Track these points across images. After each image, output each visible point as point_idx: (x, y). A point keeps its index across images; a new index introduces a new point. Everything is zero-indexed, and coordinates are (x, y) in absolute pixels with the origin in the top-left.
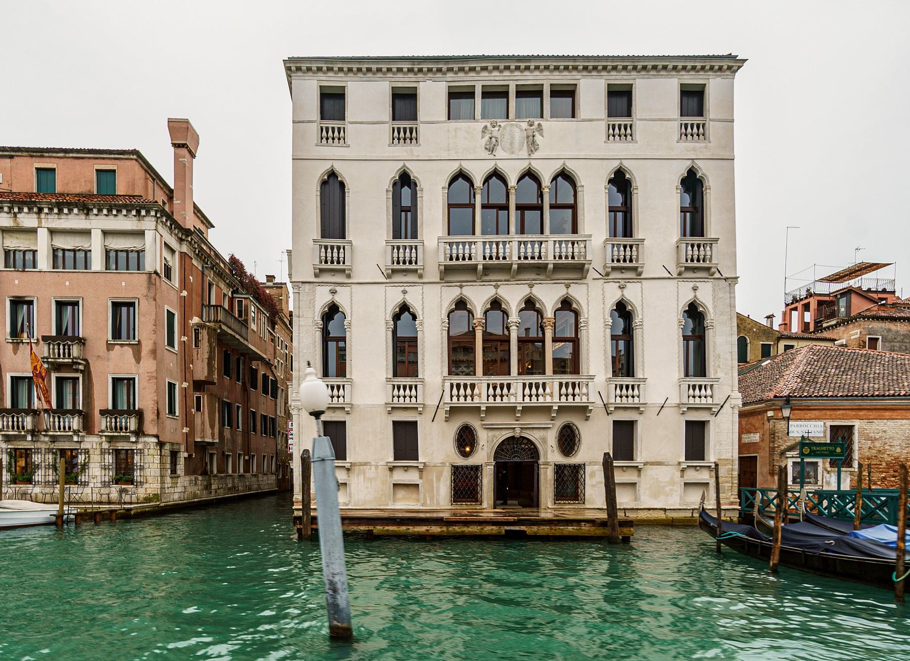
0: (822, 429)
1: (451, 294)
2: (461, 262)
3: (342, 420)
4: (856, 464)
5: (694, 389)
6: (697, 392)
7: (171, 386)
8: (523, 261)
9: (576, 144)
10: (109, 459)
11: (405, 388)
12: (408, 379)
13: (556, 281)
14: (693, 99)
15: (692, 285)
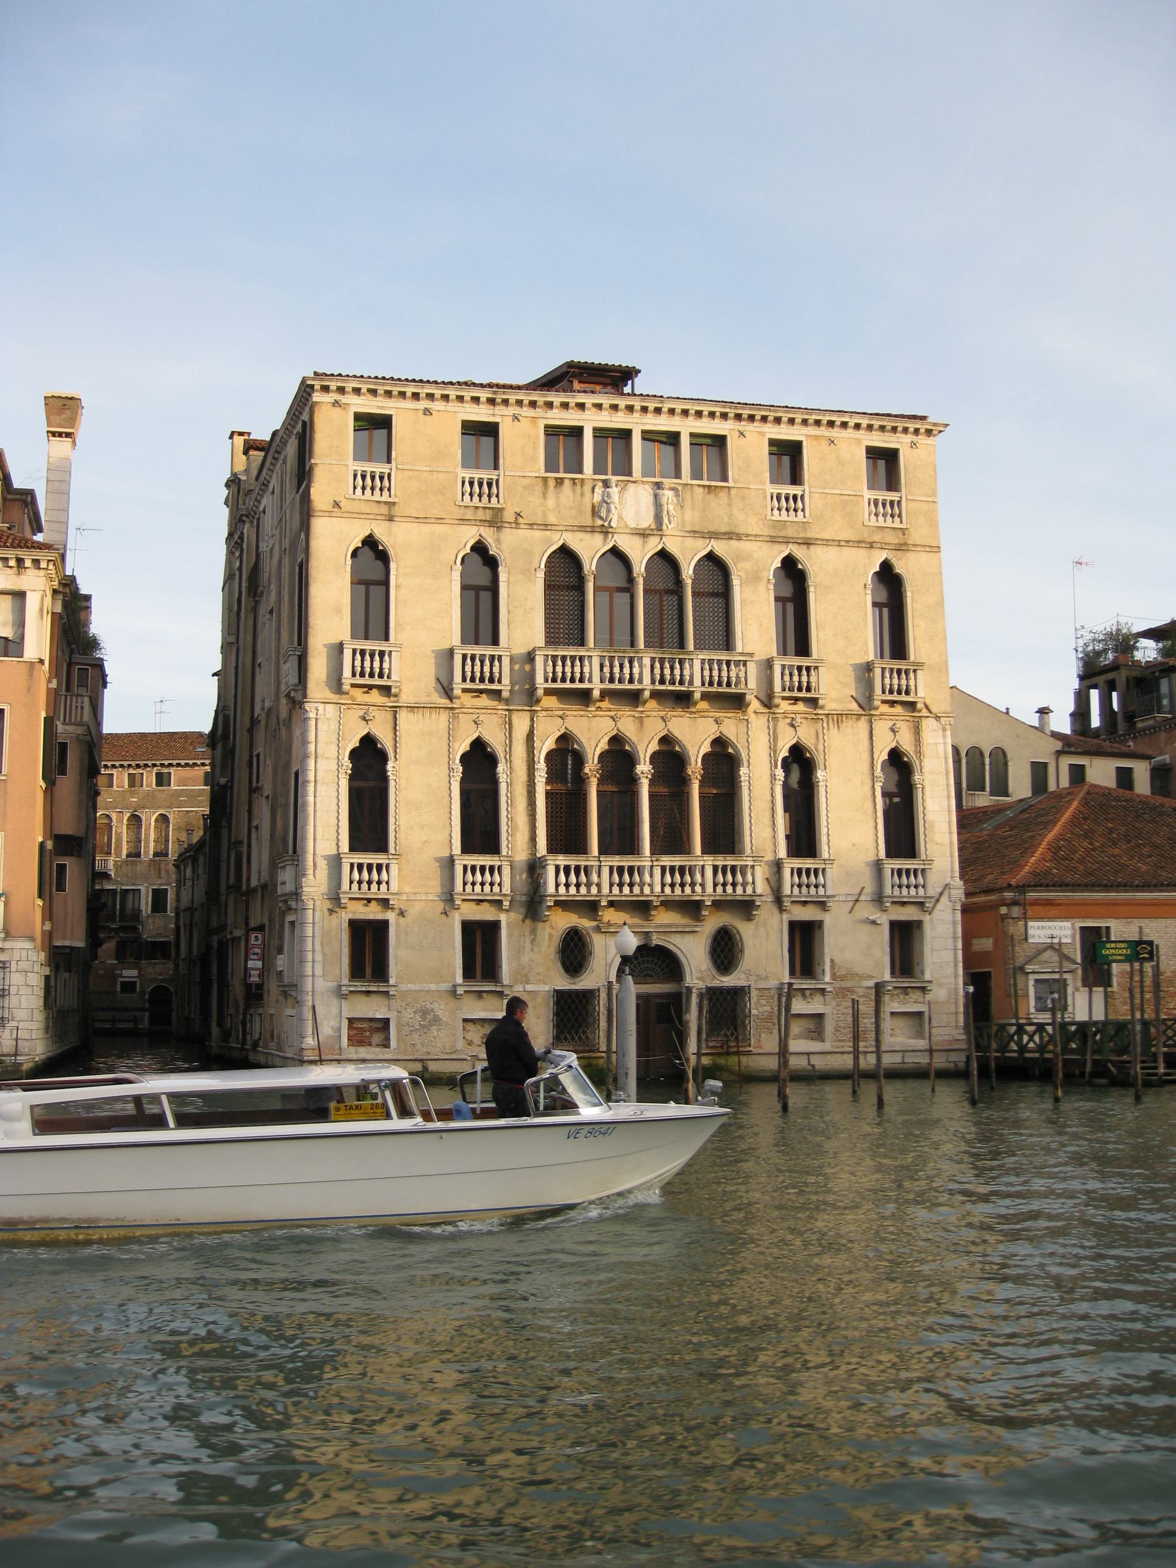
0: (1069, 932)
2: (568, 685)
5: (900, 875)
6: (904, 880)
9: (742, 522)
12: (481, 857)
14: (885, 463)
15: (890, 723)
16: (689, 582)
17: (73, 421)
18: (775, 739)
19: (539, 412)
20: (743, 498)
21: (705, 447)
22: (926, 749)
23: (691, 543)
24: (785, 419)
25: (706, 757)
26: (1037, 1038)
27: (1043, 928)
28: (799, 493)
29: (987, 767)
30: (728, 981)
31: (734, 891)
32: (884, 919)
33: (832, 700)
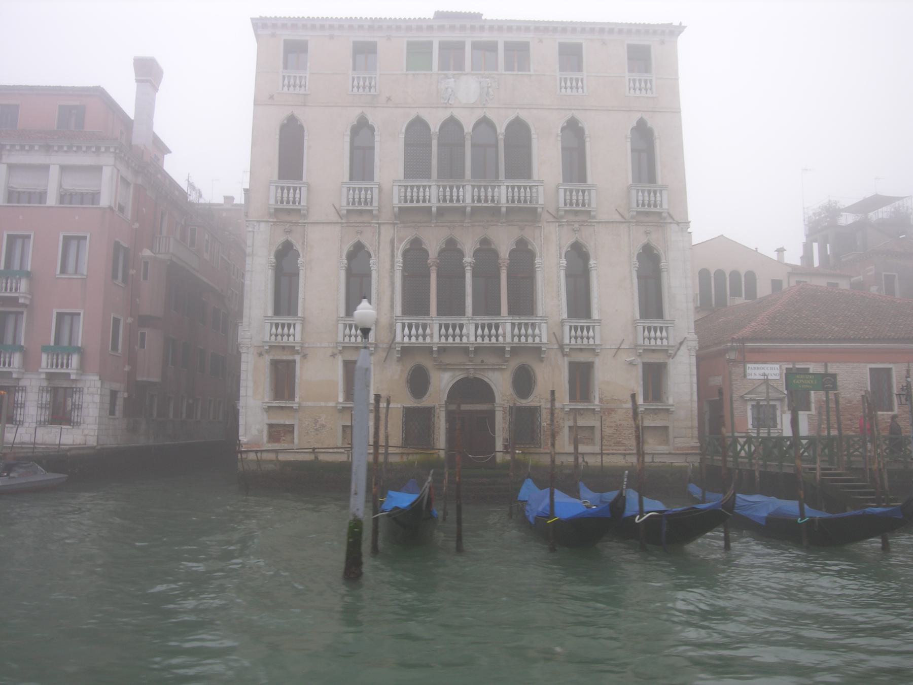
0: (778, 372)
1: (408, 235)
2: (415, 204)
3: (590, 360)
4: (813, 406)
7: (116, 322)
8: (476, 204)
10: (46, 398)
16: (501, 137)
26: (746, 447)
28: (580, 77)
30: (524, 403)
32: (639, 361)
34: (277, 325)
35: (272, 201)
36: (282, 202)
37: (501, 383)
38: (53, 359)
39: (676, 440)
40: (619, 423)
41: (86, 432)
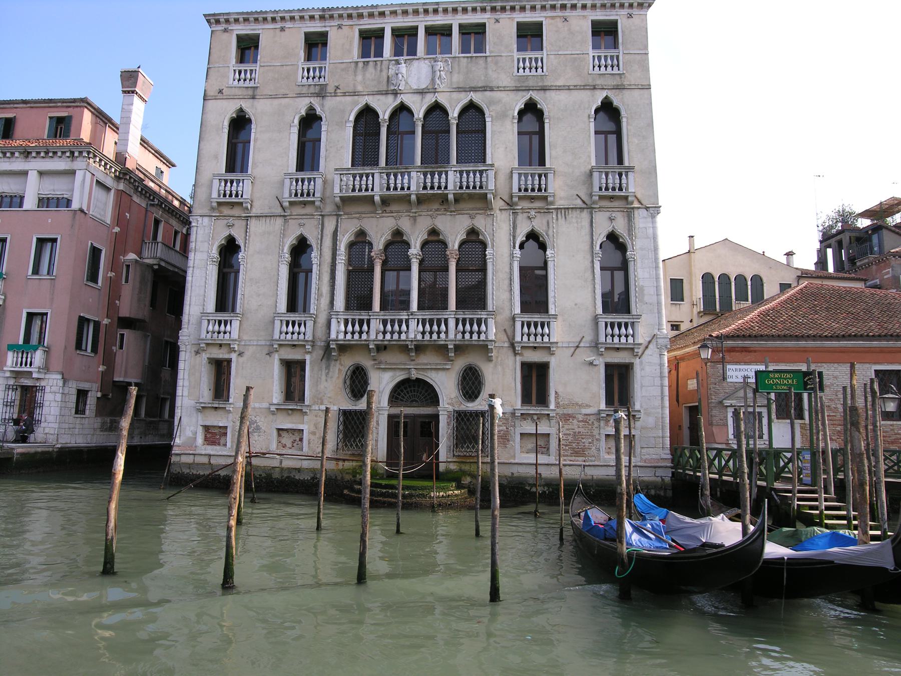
11: (220, 322)
13: (459, 212)
16: (454, 123)
17: (135, 84)
18: (515, 228)
19: (355, 21)
20: (496, 63)
21: (473, 35)
22: (638, 232)
23: (455, 95)
24: (528, 7)
25: (462, 243)
27: (740, 370)
28: (539, 56)
29: (749, 287)
31: (471, 337)
32: (600, 362)
33: (561, 198)
34: (220, 322)
35: (215, 195)
36: (225, 195)
37: (447, 385)
38: (17, 358)
39: (644, 451)
40: (577, 430)
41: (47, 431)
